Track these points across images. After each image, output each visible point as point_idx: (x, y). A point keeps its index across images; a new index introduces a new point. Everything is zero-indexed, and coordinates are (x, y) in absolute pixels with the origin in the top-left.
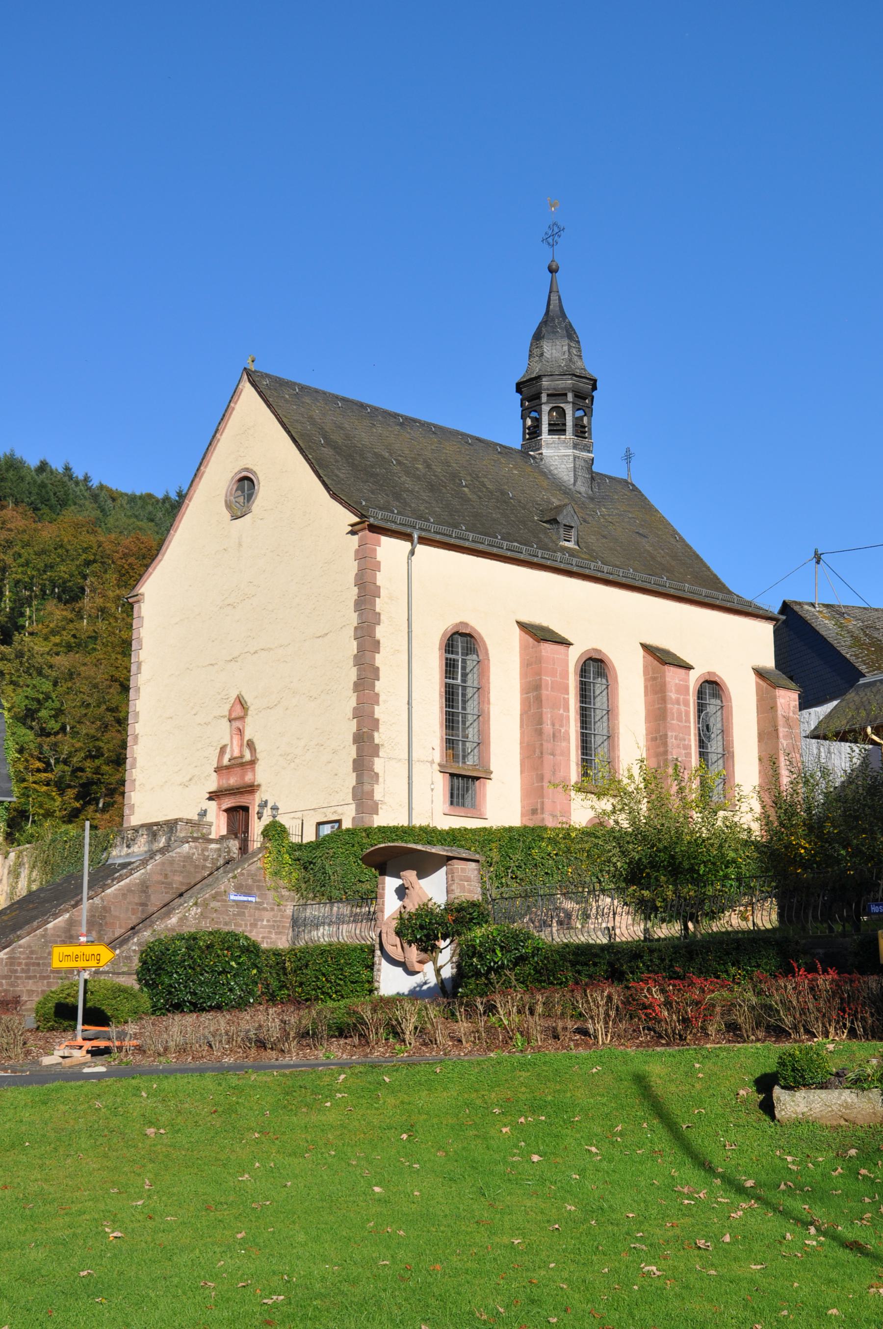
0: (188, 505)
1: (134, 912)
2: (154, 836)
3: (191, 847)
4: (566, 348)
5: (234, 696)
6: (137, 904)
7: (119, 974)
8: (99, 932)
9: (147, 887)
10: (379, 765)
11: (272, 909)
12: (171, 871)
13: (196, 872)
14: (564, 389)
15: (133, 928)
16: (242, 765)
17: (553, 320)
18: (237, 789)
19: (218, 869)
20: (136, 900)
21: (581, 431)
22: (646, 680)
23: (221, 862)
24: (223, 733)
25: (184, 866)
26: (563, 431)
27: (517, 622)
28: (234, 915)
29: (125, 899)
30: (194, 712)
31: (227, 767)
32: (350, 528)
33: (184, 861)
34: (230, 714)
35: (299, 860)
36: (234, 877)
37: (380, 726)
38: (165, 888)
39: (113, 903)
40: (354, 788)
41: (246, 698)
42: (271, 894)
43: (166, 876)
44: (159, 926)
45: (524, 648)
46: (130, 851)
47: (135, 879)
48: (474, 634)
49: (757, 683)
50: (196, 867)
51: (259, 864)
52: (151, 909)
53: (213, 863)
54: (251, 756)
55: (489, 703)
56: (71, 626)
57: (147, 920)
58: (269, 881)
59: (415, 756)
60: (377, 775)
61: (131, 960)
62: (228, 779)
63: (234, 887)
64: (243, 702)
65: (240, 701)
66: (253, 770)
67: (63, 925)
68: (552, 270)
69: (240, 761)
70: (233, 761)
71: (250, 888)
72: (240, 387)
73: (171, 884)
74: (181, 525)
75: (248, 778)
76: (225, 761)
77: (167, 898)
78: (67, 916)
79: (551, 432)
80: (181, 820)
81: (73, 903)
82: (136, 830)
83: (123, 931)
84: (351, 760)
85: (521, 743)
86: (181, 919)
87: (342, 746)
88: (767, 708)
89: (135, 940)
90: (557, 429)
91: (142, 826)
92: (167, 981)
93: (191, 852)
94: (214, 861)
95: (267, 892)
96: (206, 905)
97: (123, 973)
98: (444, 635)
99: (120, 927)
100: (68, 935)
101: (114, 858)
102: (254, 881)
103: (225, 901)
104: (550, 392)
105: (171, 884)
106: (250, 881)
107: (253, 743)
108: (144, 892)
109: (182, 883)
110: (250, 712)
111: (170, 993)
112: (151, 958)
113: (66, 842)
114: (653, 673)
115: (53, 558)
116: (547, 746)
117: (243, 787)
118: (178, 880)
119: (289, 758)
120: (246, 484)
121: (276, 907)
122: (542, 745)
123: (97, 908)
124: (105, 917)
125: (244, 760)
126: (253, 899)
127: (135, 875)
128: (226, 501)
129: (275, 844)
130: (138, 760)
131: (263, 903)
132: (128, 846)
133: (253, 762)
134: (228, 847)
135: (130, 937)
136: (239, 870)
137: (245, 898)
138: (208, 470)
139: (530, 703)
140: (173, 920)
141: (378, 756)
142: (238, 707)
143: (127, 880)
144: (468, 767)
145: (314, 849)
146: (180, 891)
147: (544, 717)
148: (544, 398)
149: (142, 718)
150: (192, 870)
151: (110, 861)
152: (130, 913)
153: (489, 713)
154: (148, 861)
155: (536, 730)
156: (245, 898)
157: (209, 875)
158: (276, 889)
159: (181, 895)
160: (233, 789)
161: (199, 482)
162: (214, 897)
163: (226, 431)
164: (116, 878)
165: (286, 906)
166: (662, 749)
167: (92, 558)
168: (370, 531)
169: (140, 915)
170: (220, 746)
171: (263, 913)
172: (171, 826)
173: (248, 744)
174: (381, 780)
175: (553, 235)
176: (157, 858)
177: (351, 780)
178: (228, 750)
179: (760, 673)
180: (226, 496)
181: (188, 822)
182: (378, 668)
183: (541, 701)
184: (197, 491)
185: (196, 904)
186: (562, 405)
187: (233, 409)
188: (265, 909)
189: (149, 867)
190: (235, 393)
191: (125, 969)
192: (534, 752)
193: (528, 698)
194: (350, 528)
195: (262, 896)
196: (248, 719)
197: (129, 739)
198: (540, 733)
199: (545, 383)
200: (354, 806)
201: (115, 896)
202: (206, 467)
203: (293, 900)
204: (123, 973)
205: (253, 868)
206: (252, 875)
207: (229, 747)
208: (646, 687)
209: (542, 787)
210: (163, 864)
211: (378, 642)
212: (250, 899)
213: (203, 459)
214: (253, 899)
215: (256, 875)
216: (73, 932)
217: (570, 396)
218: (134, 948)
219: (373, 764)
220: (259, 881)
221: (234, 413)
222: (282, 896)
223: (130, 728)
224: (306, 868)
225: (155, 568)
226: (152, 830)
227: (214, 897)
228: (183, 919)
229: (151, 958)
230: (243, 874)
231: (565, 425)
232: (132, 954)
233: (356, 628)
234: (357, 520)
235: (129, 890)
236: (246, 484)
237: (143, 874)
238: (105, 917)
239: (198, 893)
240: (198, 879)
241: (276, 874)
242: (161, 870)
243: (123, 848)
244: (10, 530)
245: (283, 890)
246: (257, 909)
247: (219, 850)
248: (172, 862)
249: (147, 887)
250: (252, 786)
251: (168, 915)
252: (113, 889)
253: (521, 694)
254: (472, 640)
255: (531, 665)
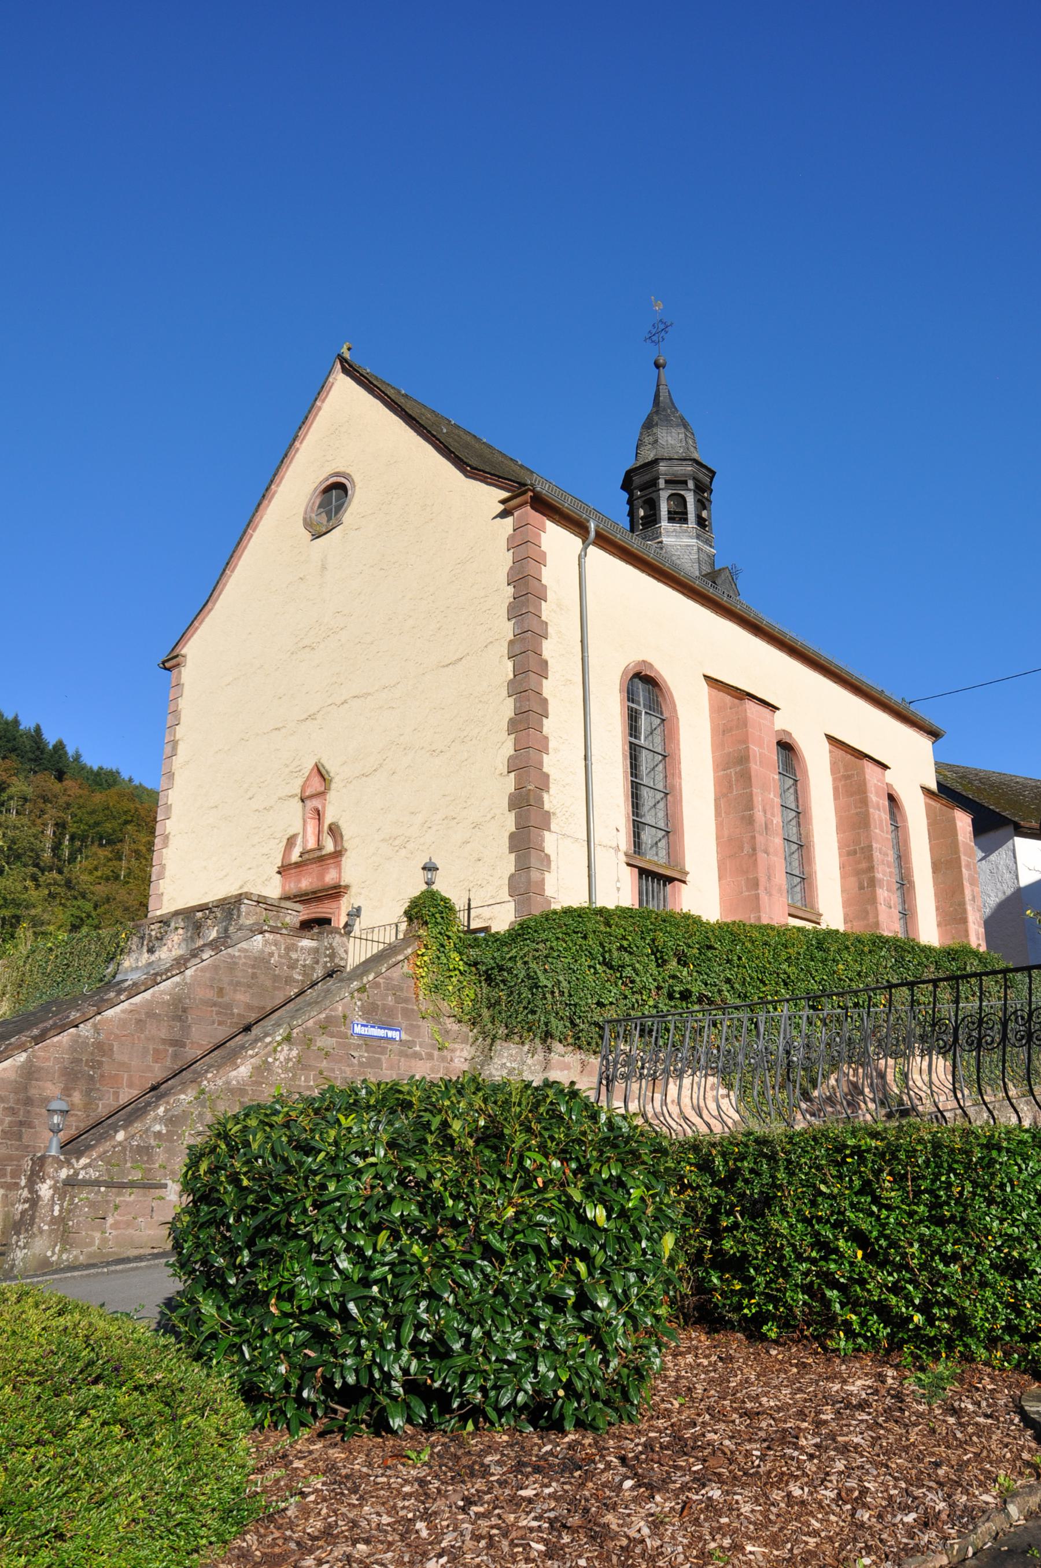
0: (252, 536)
1: (158, 1056)
2: (197, 928)
3: (266, 942)
4: (682, 436)
5: (310, 765)
6: (164, 1041)
7: (122, 1186)
8: (88, 1093)
9: (185, 1010)
10: (550, 842)
11: (430, 1056)
12: (231, 983)
13: (275, 988)
14: (685, 475)
15: (154, 1088)
16: (322, 859)
17: (664, 410)
18: (314, 893)
19: (313, 985)
20: (163, 1034)
21: (701, 522)
22: (834, 780)
23: (319, 972)
24: (292, 818)
25: (254, 976)
26: (685, 520)
27: (705, 676)
28: (361, 1064)
29: (142, 1031)
30: (250, 794)
31: (297, 865)
32: (502, 507)
33: (253, 967)
34: (303, 790)
35: (475, 964)
36: (362, 989)
37: (551, 785)
38: (218, 1013)
39: (117, 1037)
40: (511, 877)
41: (328, 767)
42: (427, 1027)
43: (221, 991)
44: (213, 1082)
45: (716, 710)
46: (153, 958)
47: (162, 992)
48: (659, 681)
49: (927, 804)
50: (276, 978)
51: (407, 968)
52: (192, 1052)
53: (305, 974)
54: (335, 846)
55: (680, 777)
56: (110, 864)
57: (183, 1072)
58: (425, 1005)
59: (598, 835)
60: (548, 856)
61: (150, 1156)
62: (299, 881)
63: (362, 1008)
64: (324, 772)
65: (320, 772)
66: (339, 866)
67: (12, 1076)
68: (657, 366)
69: (317, 854)
70: (306, 856)
71: (390, 1012)
72: (331, 379)
73: (229, 1006)
74: (241, 563)
75: (330, 877)
76: (295, 857)
77: (222, 1033)
78: (22, 1057)
79: (671, 520)
80: (248, 896)
81: (35, 1032)
82: (164, 921)
83: (136, 1092)
84: (507, 834)
85: (717, 838)
86: (257, 1070)
87: (489, 816)
88: (941, 835)
89: (161, 1110)
90: (678, 516)
91: (176, 913)
92: (307, 1288)
93: (267, 950)
94: (307, 970)
95: (421, 1022)
96: (308, 1042)
97: (132, 1185)
98: (625, 672)
99: (130, 1085)
100: (22, 1096)
101: (126, 972)
102: (398, 1000)
103: (345, 1036)
104: (668, 477)
105: (229, 1006)
106: (390, 1000)
107: (338, 827)
108: (179, 1018)
109: (249, 1007)
110: (333, 786)
111: (320, 1337)
112: (234, 1179)
113: (51, 949)
114: (846, 770)
115: (99, 817)
116: (760, 839)
117: (320, 891)
118: (242, 1001)
119: (397, 842)
120: (335, 493)
121: (436, 1053)
122: (754, 837)
123: (85, 1044)
124: (100, 1063)
125: (324, 853)
126: (395, 1035)
127: (163, 986)
128: (305, 519)
129: (435, 931)
130: (168, 867)
131: (413, 1043)
132: (151, 951)
133: (338, 854)
134: (331, 947)
135: (148, 1104)
136: (371, 977)
137: (381, 1033)
138: (281, 489)
139: (730, 782)
140: (243, 1071)
141: (549, 830)
142: (316, 781)
143: (147, 995)
144: (656, 859)
145: (506, 944)
146: (246, 1021)
147: (755, 798)
148: (662, 483)
149: (175, 812)
150: (268, 983)
151: (119, 978)
152: (150, 1058)
153: (681, 790)
154: (187, 960)
155: (743, 818)
156: (381, 1033)
157: (298, 995)
158: (436, 1018)
159: (247, 1029)
160: (306, 894)
161: (268, 506)
162: (324, 1027)
163: (308, 437)
164: (125, 990)
165: (453, 1051)
166: (864, 865)
167: (130, 818)
168: (532, 508)
169: (171, 1064)
170: (288, 836)
171: (413, 1062)
172: (229, 908)
173: (330, 829)
174: (553, 865)
175: (658, 332)
176: (205, 956)
177: (508, 864)
178: (299, 840)
179: (926, 791)
180: (305, 513)
181: (261, 901)
182: (546, 700)
183: (750, 778)
184: (265, 517)
185: (288, 1039)
186: (682, 492)
187: (320, 408)
188: (417, 1056)
189: (188, 973)
190: (320, 389)
191: (136, 1176)
192: (742, 849)
193: (729, 776)
194: (502, 507)
195: (412, 1029)
196: (332, 796)
197: (156, 841)
198: (750, 821)
199: (662, 467)
200: (513, 904)
201: (123, 1023)
202: (278, 486)
203: (465, 1041)
204: (132, 1185)
205: (396, 973)
206: (395, 989)
207: (300, 836)
208: (836, 789)
209: (757, 897)
210: (216, 968)
211: (546, 662)
212: (390, 1034)
213: (275, 475)
214: (395, 1035)
215: (401, 989)
216: (33, 1092)
217: (691, 484)
218: (157, 1128)
219: (543, 841)
220: (406, 1000)
221: (321, 413)
222: (447, 1032)
223: (158, 826)
224: (489, 980)
225: (202, 621)
226: (193, 918)
227: (324, 1027)
228: (262, 1070)
229: (234, 1179)
230: (377, 985)
231: (686, 513)
232: (153, 1142)
233: (511, 643)
234: (505, 495)
235: (150, 1013)
236: (335, 493)
237: (178, 984)
238: (100, 1063)
239: (293, 1018)
240: (278, 1002)
241: (436, 988)
242: (212, 979)
243: (141, 954)
244: (69, 796)
245: (448, 1021)
246: (402, 1054)
247: (316, 950)
248: (232, 966)
249: (185, 1010)
250: (337, 887)
251: (232, 1059)
252: (118, 1009)
253: (715, 771)
254: (656, 690)
255: (731, 730)
